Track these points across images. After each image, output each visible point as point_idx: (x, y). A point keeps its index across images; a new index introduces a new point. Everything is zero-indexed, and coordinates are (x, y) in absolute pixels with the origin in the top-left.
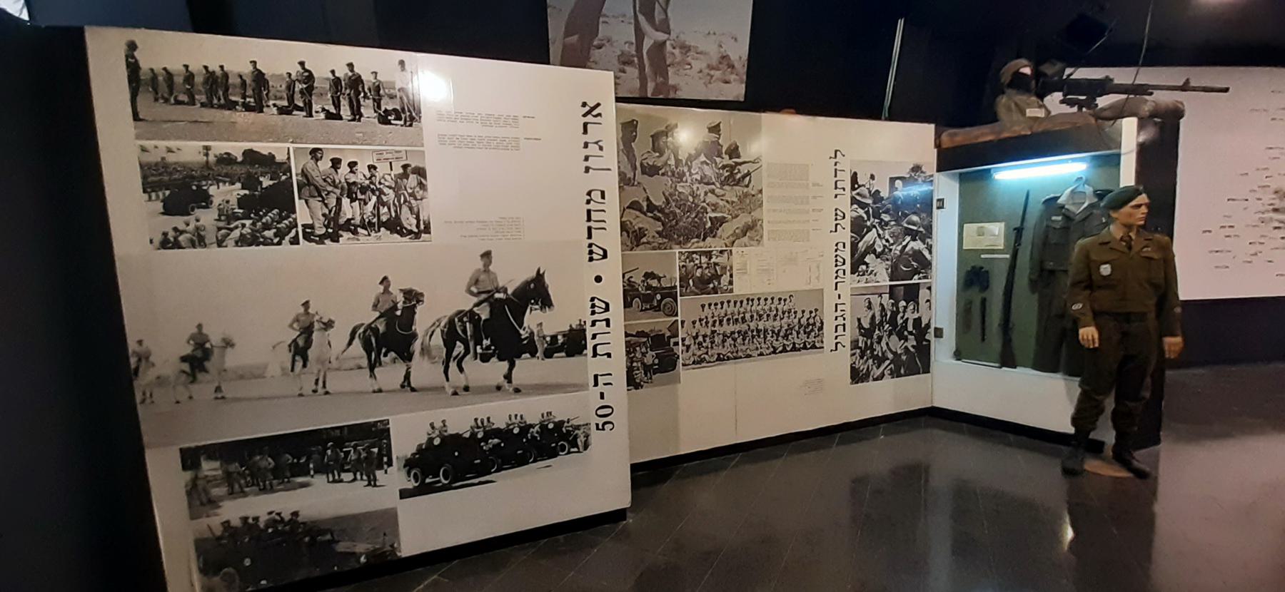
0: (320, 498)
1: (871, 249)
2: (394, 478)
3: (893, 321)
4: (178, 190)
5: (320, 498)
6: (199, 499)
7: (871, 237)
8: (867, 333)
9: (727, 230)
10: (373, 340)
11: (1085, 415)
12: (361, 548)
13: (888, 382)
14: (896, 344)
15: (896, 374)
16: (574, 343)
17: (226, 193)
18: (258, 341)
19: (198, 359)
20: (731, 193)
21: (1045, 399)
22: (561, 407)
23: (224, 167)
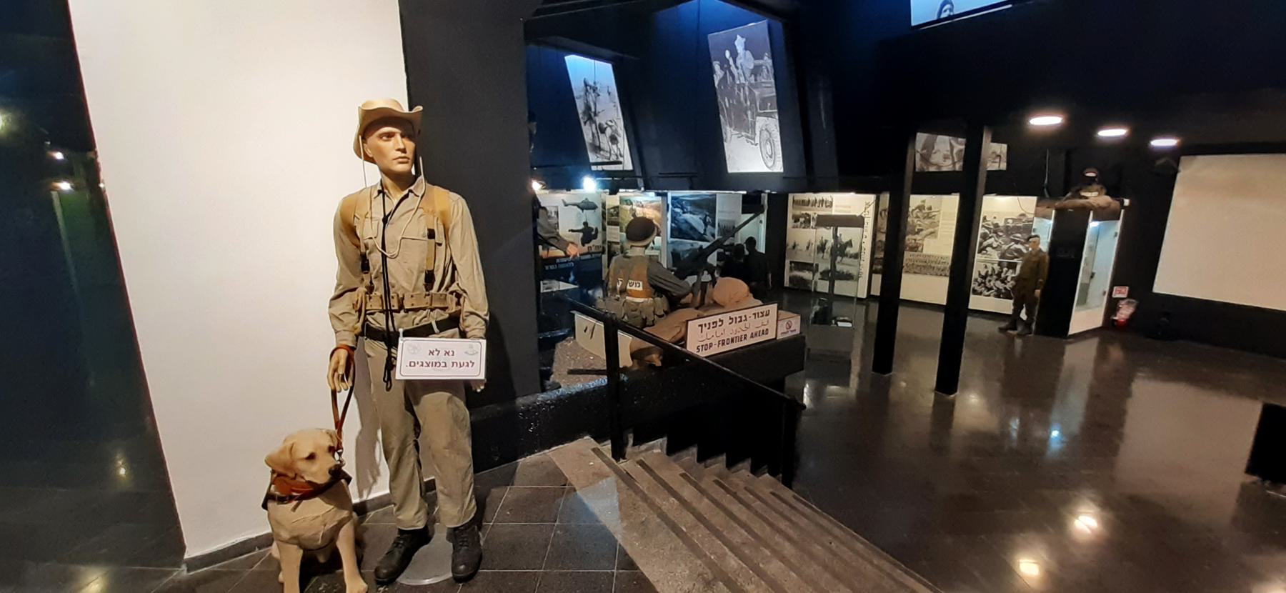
0: (807, 275)
1: (990, 245)
2: (818, 275)
3: (999, 275)
4: (796, 219)
5: (807, 275)
6: (791, 269)
7: (989, 241)
8: (984, 277)
9: (924, 233)
10: (552, 267)
11: (1017, 310)
12: (699, 562)
13: (992, 298)
14: (999, 284)
15: (998, 296)
16: (856, 256)
17: (802, 220)
18: (802, 245)
19: (794, 247)
20: (927, 221)
21: (1006, 306)
22: (853, 271)
23: (802, 216)
